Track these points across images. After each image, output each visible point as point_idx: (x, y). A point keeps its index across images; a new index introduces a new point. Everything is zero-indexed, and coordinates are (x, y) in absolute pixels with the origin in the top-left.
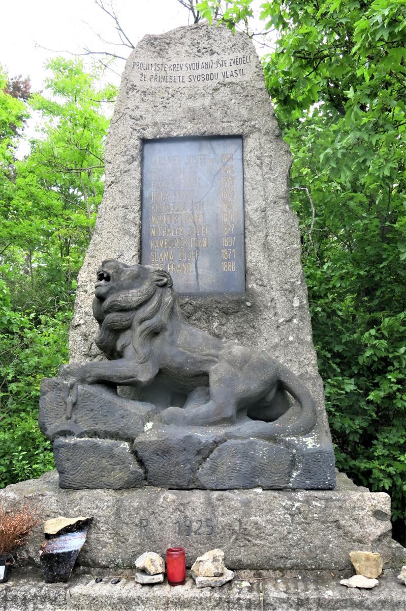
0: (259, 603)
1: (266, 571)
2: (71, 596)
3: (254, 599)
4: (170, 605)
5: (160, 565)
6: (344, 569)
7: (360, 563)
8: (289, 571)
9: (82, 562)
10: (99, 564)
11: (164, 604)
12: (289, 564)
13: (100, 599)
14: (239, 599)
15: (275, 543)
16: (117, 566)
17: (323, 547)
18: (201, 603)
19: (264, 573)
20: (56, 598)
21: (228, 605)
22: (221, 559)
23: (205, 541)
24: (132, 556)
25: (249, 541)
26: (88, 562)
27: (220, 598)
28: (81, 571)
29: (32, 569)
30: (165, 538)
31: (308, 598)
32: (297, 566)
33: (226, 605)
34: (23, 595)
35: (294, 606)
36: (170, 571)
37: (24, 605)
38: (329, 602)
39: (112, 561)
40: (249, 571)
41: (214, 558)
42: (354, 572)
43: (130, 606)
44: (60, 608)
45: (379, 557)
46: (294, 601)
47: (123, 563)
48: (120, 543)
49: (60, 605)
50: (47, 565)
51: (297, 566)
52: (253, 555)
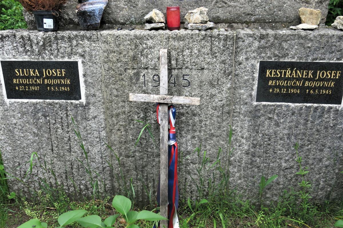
0: (233, 38)
1: (236, 24)
2: (101, 35)
3: (230, 35)
4: (170, 40)
5: (162, 17)
6: (292, 22)
7: (306, 15)
8: (253, 24)
9: (107, 20)
10: (119, 21)
11: (166, 39)
12: (253, 19)
13: (121, 37)
14: (219, 35)
15: (245, 4)
16: (132, 23)
17: (279, 6)
18: (192, 38)
19: (235, 25)
20: (91, 37)
21: (211, 39)
22: (205, 12)
23: (194, 4)
24: (142, 16)
25: (226, 3)
26: (111, 21)
27: (206, 34)
28: (106, 27)
29: (73, 26)
30: (165, 3)
31: (268, 34)
32: (258, 20)
33: (209, 38)
34: (68, 36)
35: (257, 39)
36: (170, 20)
37: (70, 42)
38: (283, 36)
39: (128, 20)
40: (224, 24)
41: (201, 12)
42: (300, 22)
43: (143, 41)
44: (95, 43)
45: (320, 12)
46: (258, 36)
47: (135, 21)
48: (132, 7)
49: (94, 41)
50: (82, 19)
51: (258, 20)
52: (228, 14)
